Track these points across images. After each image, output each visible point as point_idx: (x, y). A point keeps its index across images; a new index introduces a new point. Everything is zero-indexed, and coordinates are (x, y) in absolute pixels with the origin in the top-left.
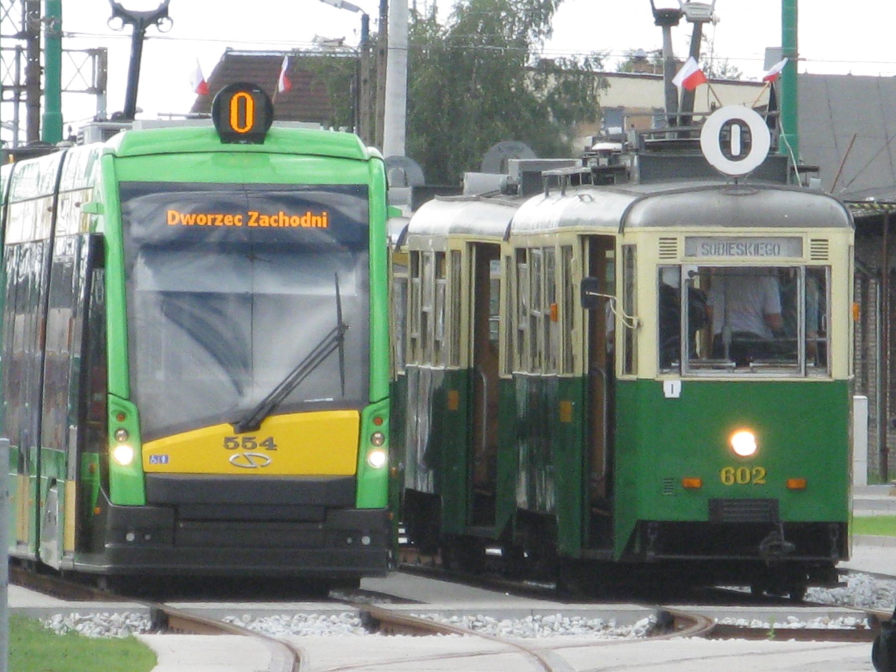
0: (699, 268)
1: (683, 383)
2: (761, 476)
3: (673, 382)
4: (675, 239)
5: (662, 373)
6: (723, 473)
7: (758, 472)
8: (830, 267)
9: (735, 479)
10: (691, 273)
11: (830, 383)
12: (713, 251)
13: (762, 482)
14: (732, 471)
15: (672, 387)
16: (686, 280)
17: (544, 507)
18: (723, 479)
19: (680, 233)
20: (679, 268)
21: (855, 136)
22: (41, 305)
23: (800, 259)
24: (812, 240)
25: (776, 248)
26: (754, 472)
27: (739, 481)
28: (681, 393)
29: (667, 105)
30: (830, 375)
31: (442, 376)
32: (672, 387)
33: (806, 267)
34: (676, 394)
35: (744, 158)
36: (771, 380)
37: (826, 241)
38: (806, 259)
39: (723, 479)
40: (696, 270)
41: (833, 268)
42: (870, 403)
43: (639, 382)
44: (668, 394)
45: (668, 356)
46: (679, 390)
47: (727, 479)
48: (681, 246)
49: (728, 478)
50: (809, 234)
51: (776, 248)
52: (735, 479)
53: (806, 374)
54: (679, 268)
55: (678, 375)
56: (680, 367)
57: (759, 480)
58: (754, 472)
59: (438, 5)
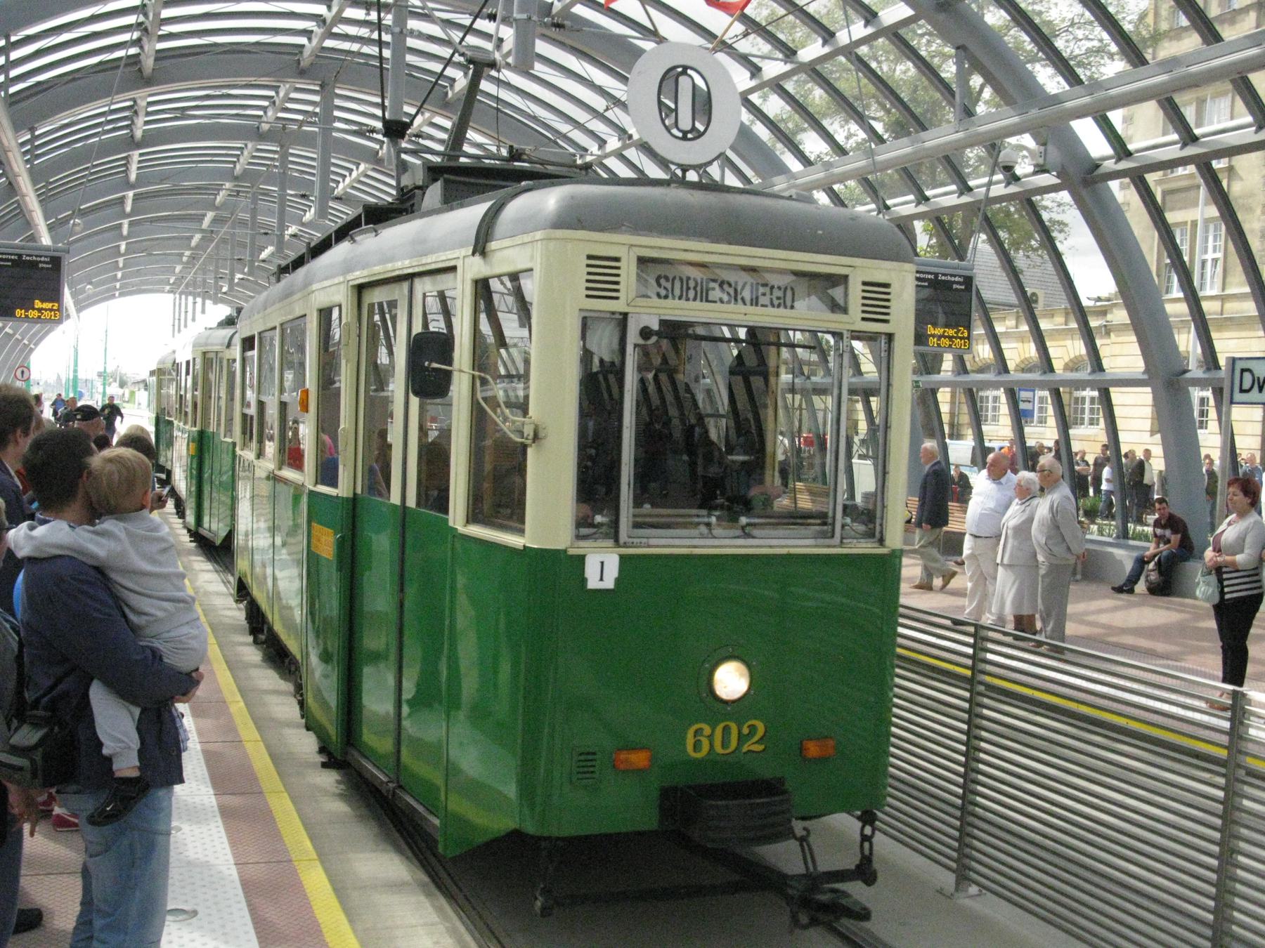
1: (622, 557)
2: (756, 738)
4: (617, 259)
5: (579, 537)
7: (753, 729)
9: (712, 745)
10: (645, 333)
11: (882, 556)
12: (677, 292)
13: (760, 748)
15: (602, 568)
17: (517, 397)
18: (690, 748)
19: (625, 247)
20: (622, 321)
24: (865, 283)
25: (789, 293)
27: (718, 749)
28: (618, 581)
29: (1188, 392)
30: (881, 541)
32: (602, 568)
34: (609, 583)
35: (1185, 526)
36: (784, 551)
39: (690, 748)
40: (655, 326)
41: (897, 338)
42: (876, 466)
44: (593, 583)
46: (615, 574)
47: (697, 746)
48: (628, 272)
49: (702, 743)
51: (789, 293)
52: (712, 745)
54: (622, 321)
55: (610, 543)
56: (615, 524)
57: (753, 746)
58: (745, 731)
59: (1095, 296)
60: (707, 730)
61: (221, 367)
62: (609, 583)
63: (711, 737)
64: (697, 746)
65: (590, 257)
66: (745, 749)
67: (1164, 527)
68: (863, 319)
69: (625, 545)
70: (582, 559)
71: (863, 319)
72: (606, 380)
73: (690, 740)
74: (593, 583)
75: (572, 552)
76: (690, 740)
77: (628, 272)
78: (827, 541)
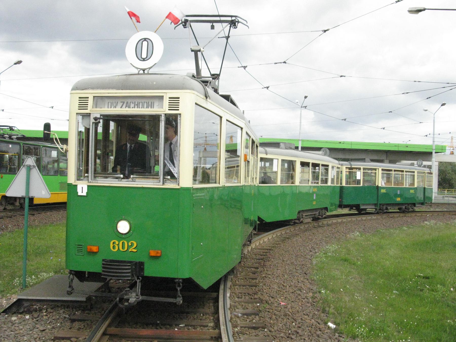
0: (101, 115)
1: (88, 186)
3: (82, 186)
4: (88, 98)
6: (112, 243)
8: (180, 114)
13: (135, 250)
14: (117, 243)
15: (82, 189)
16: (93, 123)
19: (90, 94)
21: (198, 45)
22: (366, 207)
23: (162, 110)
24: (170, 98)
26: (130, 244)
28: (87, 193)
31: (430, 196)
32: (82, 189)
33: (165, 114)
34: (84, 194)
36: (141, 186)
37: (179, 98)
38: (163, 109)
43: (328, 186)
44: (80, 193)
45: (81, 174)
47: (114, 247)
48: (90, 102)
49: (116, 248)
50: (168, 94)
53: (163, 184)
56: (88, 177)
58: (130, 244)
60: (117, 243)
61: (397, 174)
62: (84, 194)
63: (118, 245)
64: (114, 247)
65: (80, 98)
66: (130, 250)
67: (134, 282)
68: (169, 110)
69: (90, 182)
70: (76, 186)
71: (169, 110)
72: (406, 177)
73: (111, 245)
74: (80, 193)
75: (74, 184)
76: (111, 245)
77: (90, 102)
78: (158, 184)
